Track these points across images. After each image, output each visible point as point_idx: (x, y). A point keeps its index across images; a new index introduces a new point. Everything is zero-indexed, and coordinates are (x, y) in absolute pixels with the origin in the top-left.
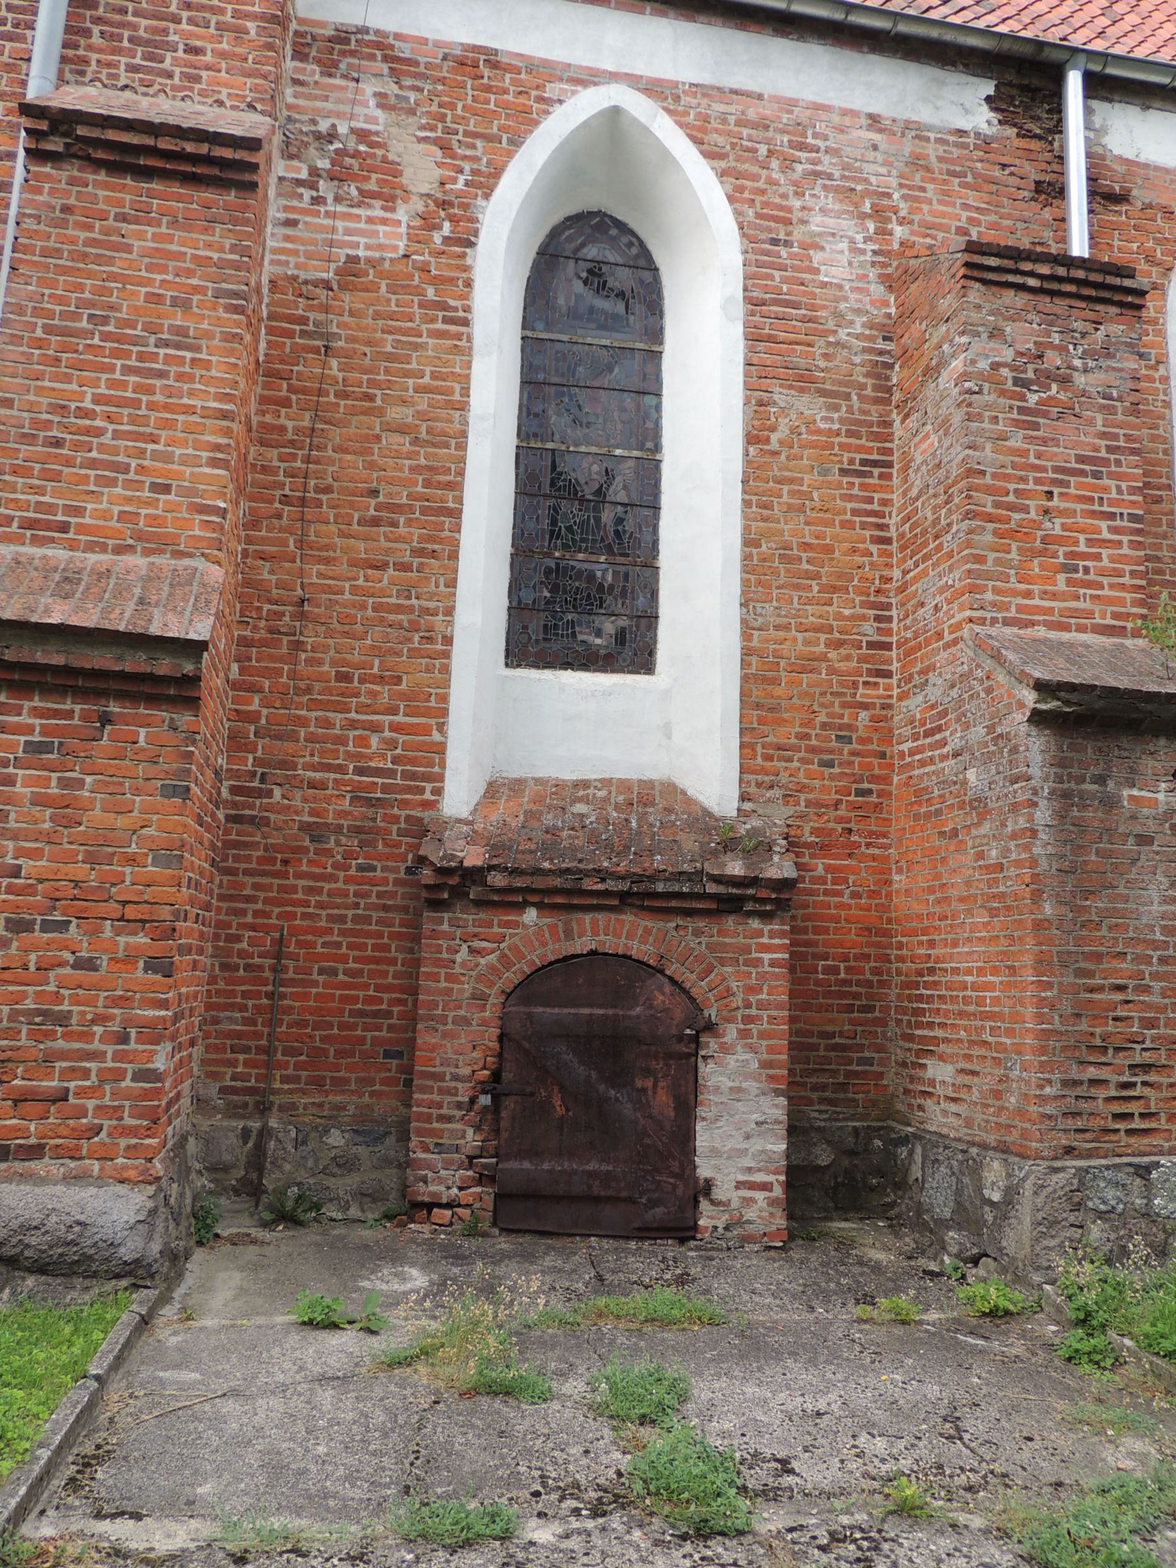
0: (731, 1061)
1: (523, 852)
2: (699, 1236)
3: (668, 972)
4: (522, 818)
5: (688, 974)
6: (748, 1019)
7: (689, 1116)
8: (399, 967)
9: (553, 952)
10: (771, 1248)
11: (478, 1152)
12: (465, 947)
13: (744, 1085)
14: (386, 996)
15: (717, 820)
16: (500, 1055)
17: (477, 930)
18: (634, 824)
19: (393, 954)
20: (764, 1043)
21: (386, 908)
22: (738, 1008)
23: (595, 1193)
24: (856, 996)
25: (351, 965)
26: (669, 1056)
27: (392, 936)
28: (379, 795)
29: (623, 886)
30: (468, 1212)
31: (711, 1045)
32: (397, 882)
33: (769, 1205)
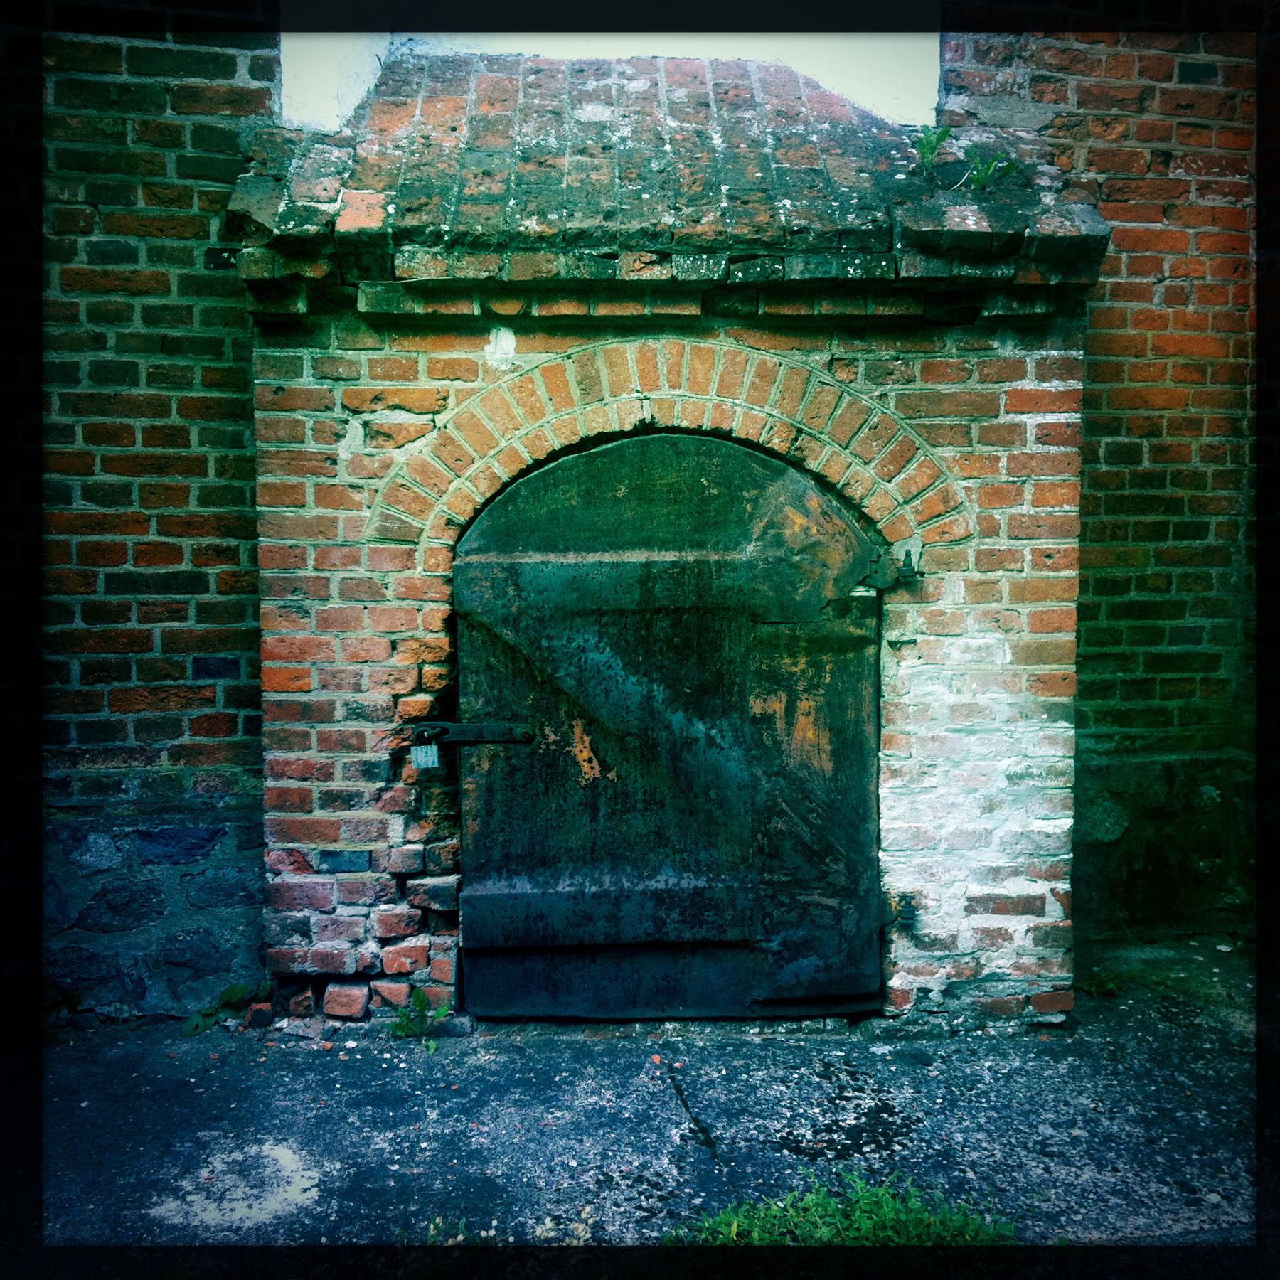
0: (954, 651)
1: (474, 200)
2: (891, 1009)
3: (812, 465)
4: (465, 132)
5: (858, 467)
6: (990, 560)
7: (865, 769)
8: (212, 478)
9: (556, 429)
10: (1040, 1026)
11: (417, 865)
12: (355, 426)
13: (982, 700)
14: (187, 543)
15: (895, 132)
16: (451, 660)
17: (379, 385)
18: (717, 141)
19: (195, 449)
20: (1026, 609)
21: (169, 346)
22: (968, 537)
23: (673, 936)
24: (1173, 505)
25: (102, 477)
26: (819, 644)
27: (187, 408)
28: (125, 78)
29: (709, 269)
30: (403, 987)
31: (907, 617)
32: (191, 285)
33: (1036, 942)
